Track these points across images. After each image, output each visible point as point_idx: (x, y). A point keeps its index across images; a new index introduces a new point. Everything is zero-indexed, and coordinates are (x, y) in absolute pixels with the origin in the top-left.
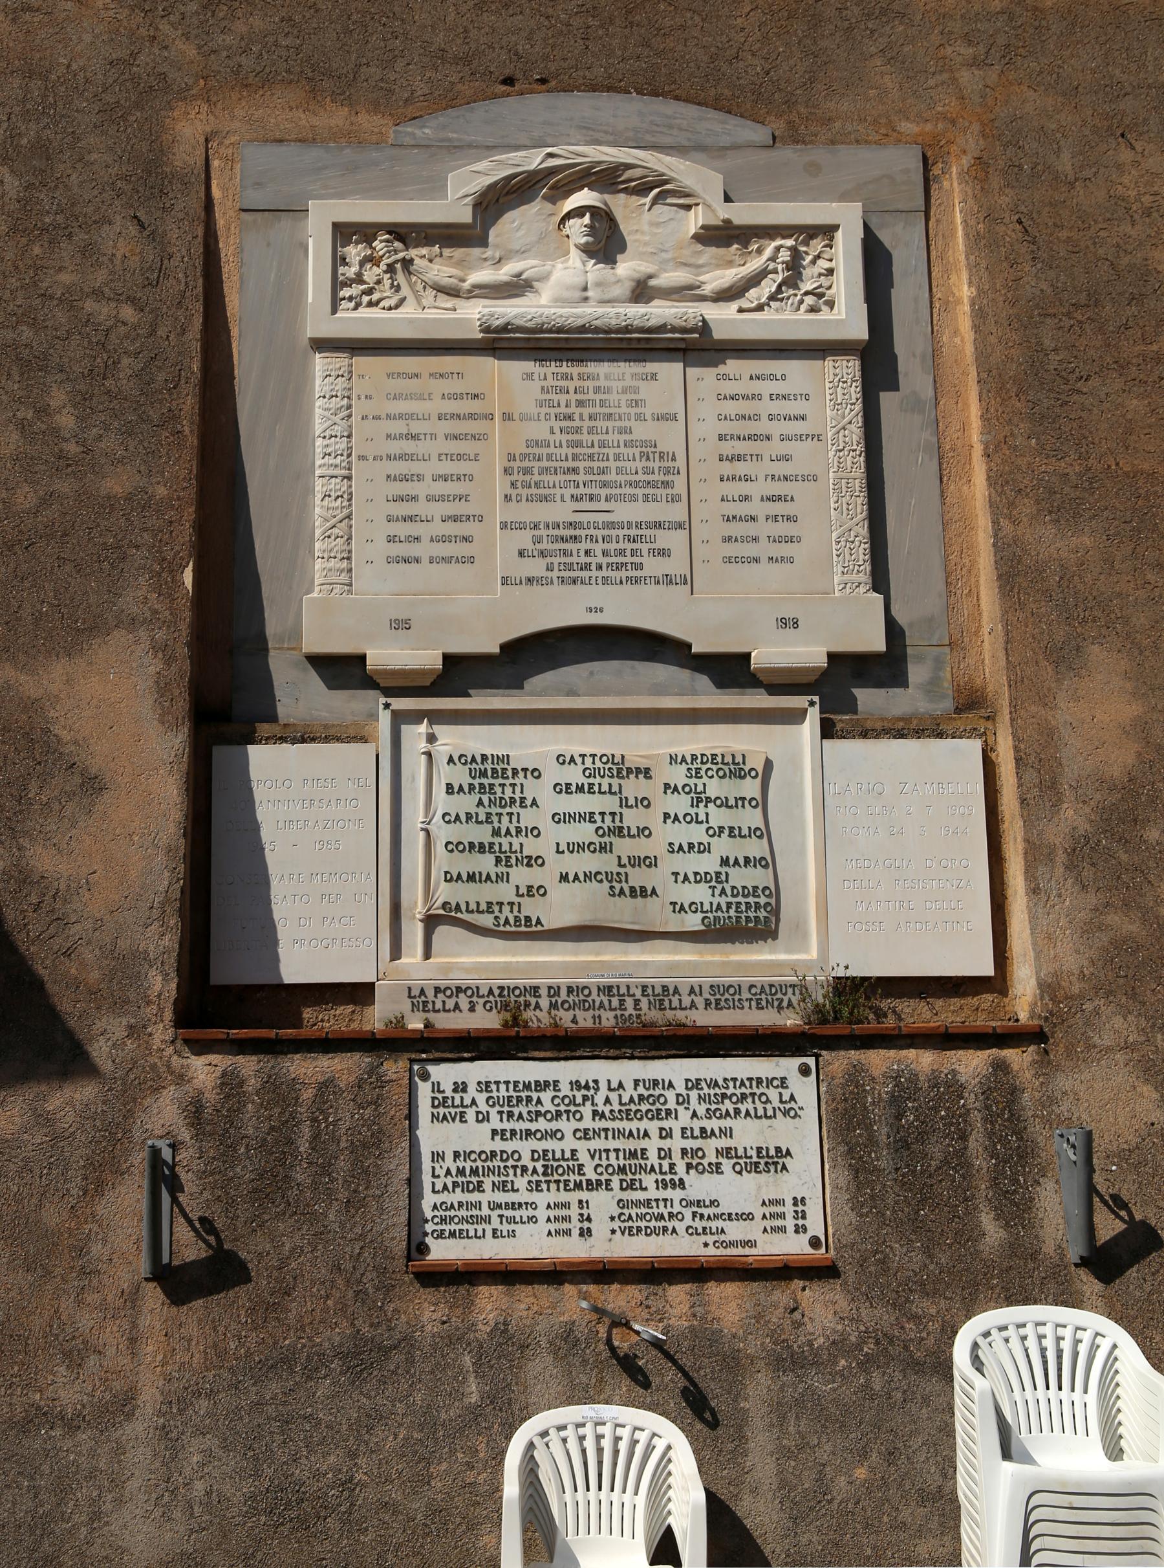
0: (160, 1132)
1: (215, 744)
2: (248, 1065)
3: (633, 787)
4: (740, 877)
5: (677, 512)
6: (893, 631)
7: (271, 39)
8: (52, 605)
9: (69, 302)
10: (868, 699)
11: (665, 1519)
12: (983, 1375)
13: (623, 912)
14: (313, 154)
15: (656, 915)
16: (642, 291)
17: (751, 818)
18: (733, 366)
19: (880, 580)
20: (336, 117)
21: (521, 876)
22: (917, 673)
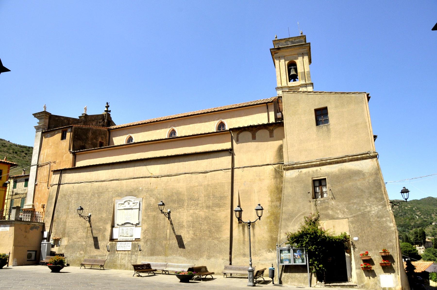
0: (45, 218)
1: (354, 237)
2: (112, 242)
3: (128, 230)
4: (132, 234)
5: (131, 217)
6: (139, 222)
7: (86, 217)
8: (356, 194)
9: (108, 208)
10: (138, 226)
11: (178, 285)
12: (215, 279)
13: (127, 235)
14: (118, 200)
15: (128, 235)
16: (130, 206)
17: (132, 231)
18: (133, 210)
19: (139, 220)
20: (119, 198)
21: (124, 234)
22: (140, 224)
